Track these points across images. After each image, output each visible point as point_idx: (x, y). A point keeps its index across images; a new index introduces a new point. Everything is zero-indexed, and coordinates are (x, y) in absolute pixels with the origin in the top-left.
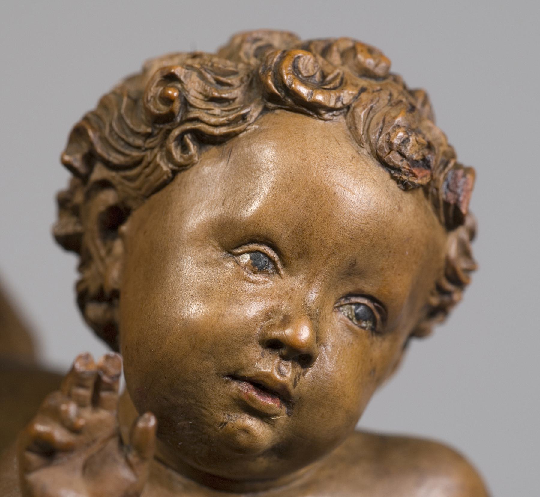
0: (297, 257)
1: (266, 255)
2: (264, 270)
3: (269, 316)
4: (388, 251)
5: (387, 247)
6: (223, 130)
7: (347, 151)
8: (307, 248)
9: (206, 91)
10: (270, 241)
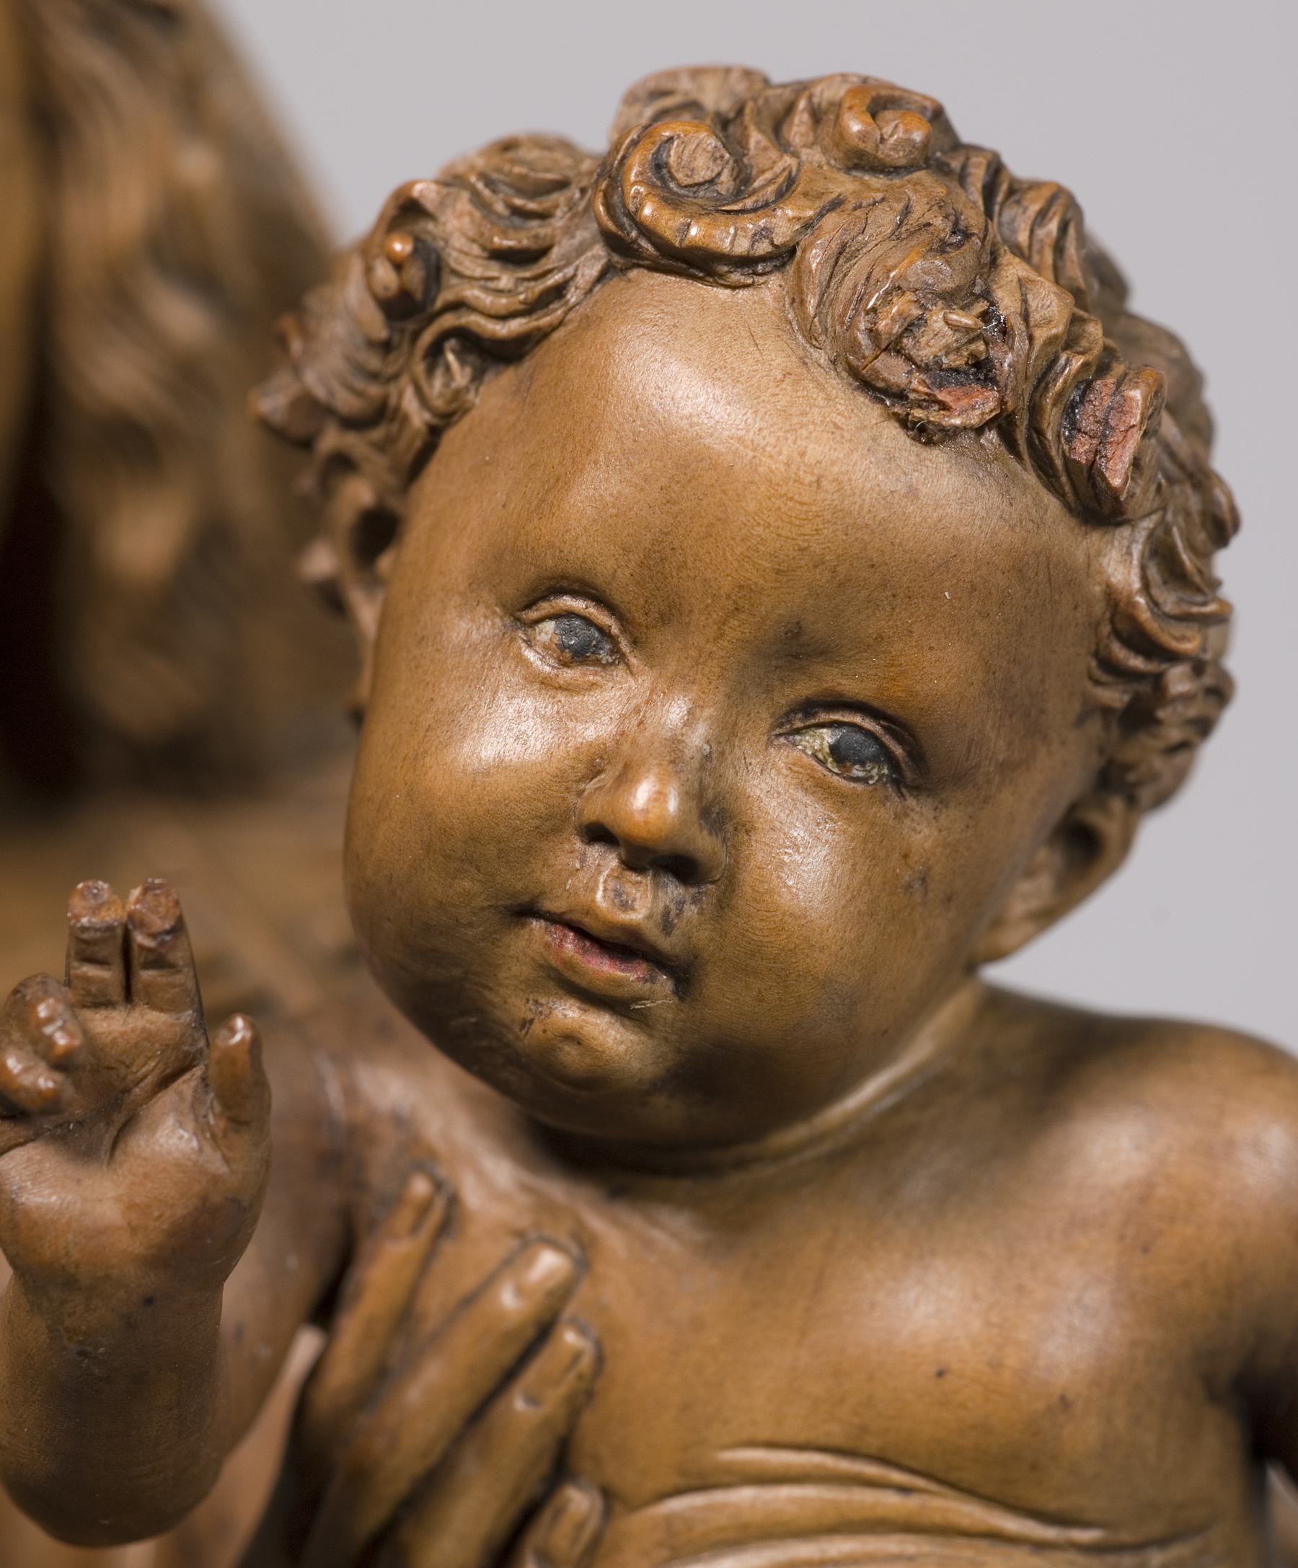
0: (657, 622)
1: (588, 621)
3: (595, 767)
4: (889, 593)
5: (884, 585)
6: (515, 326)
7: (772, 360)
8: (677, 600)
9: (482, 234)
10: (593, 588)
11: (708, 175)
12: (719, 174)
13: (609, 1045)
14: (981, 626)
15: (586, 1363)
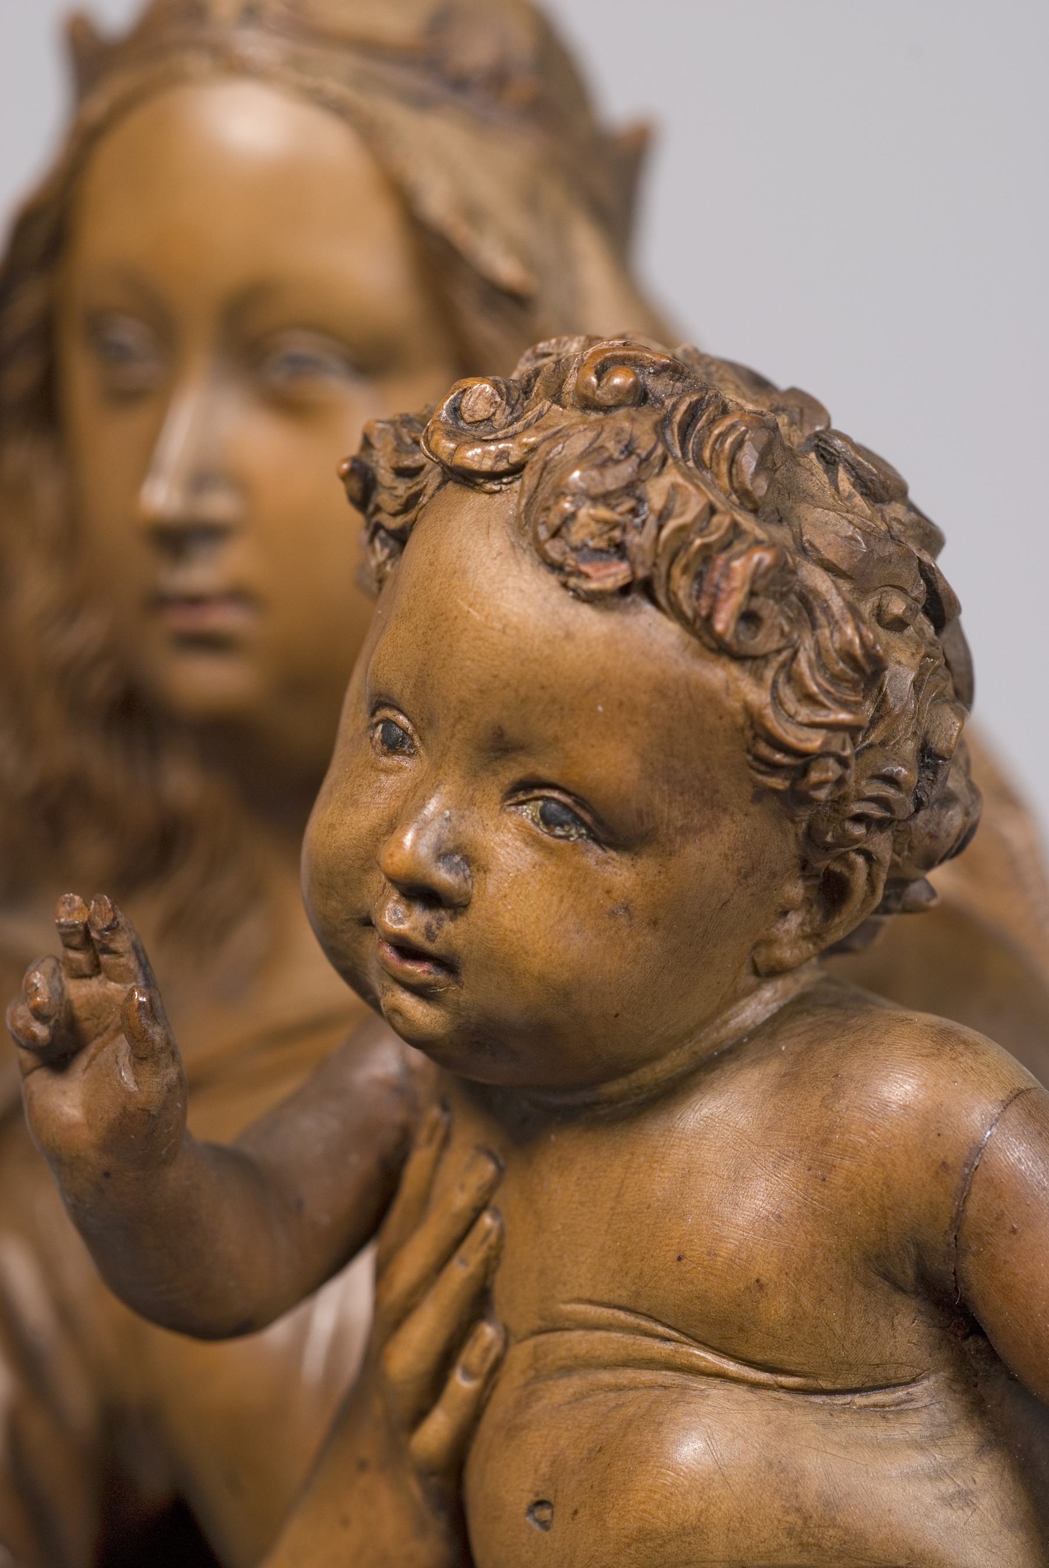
2: (397, 749)
5: (554, 700)
11: (485, 415)
12: (494, 414)
13: (418, 1017)
14: (632, 731)
15: (493, 1238)
